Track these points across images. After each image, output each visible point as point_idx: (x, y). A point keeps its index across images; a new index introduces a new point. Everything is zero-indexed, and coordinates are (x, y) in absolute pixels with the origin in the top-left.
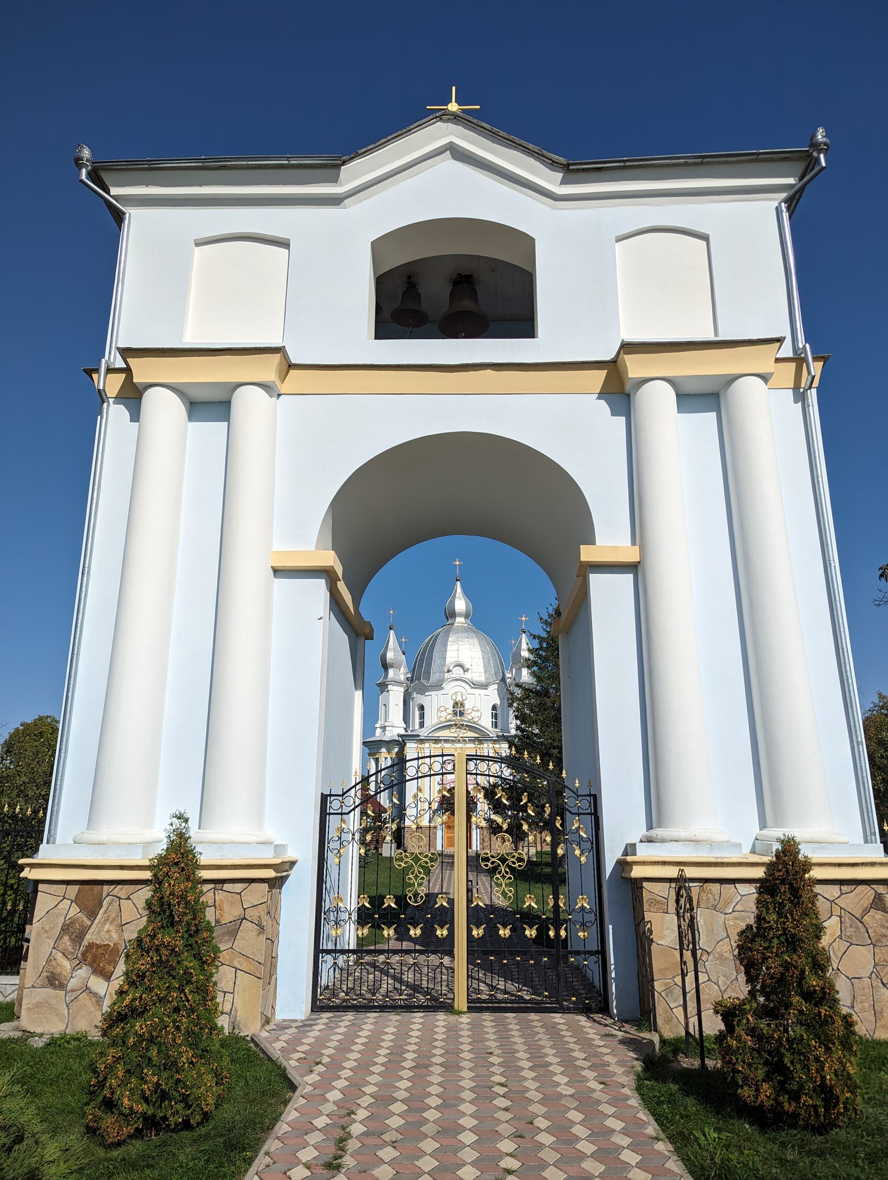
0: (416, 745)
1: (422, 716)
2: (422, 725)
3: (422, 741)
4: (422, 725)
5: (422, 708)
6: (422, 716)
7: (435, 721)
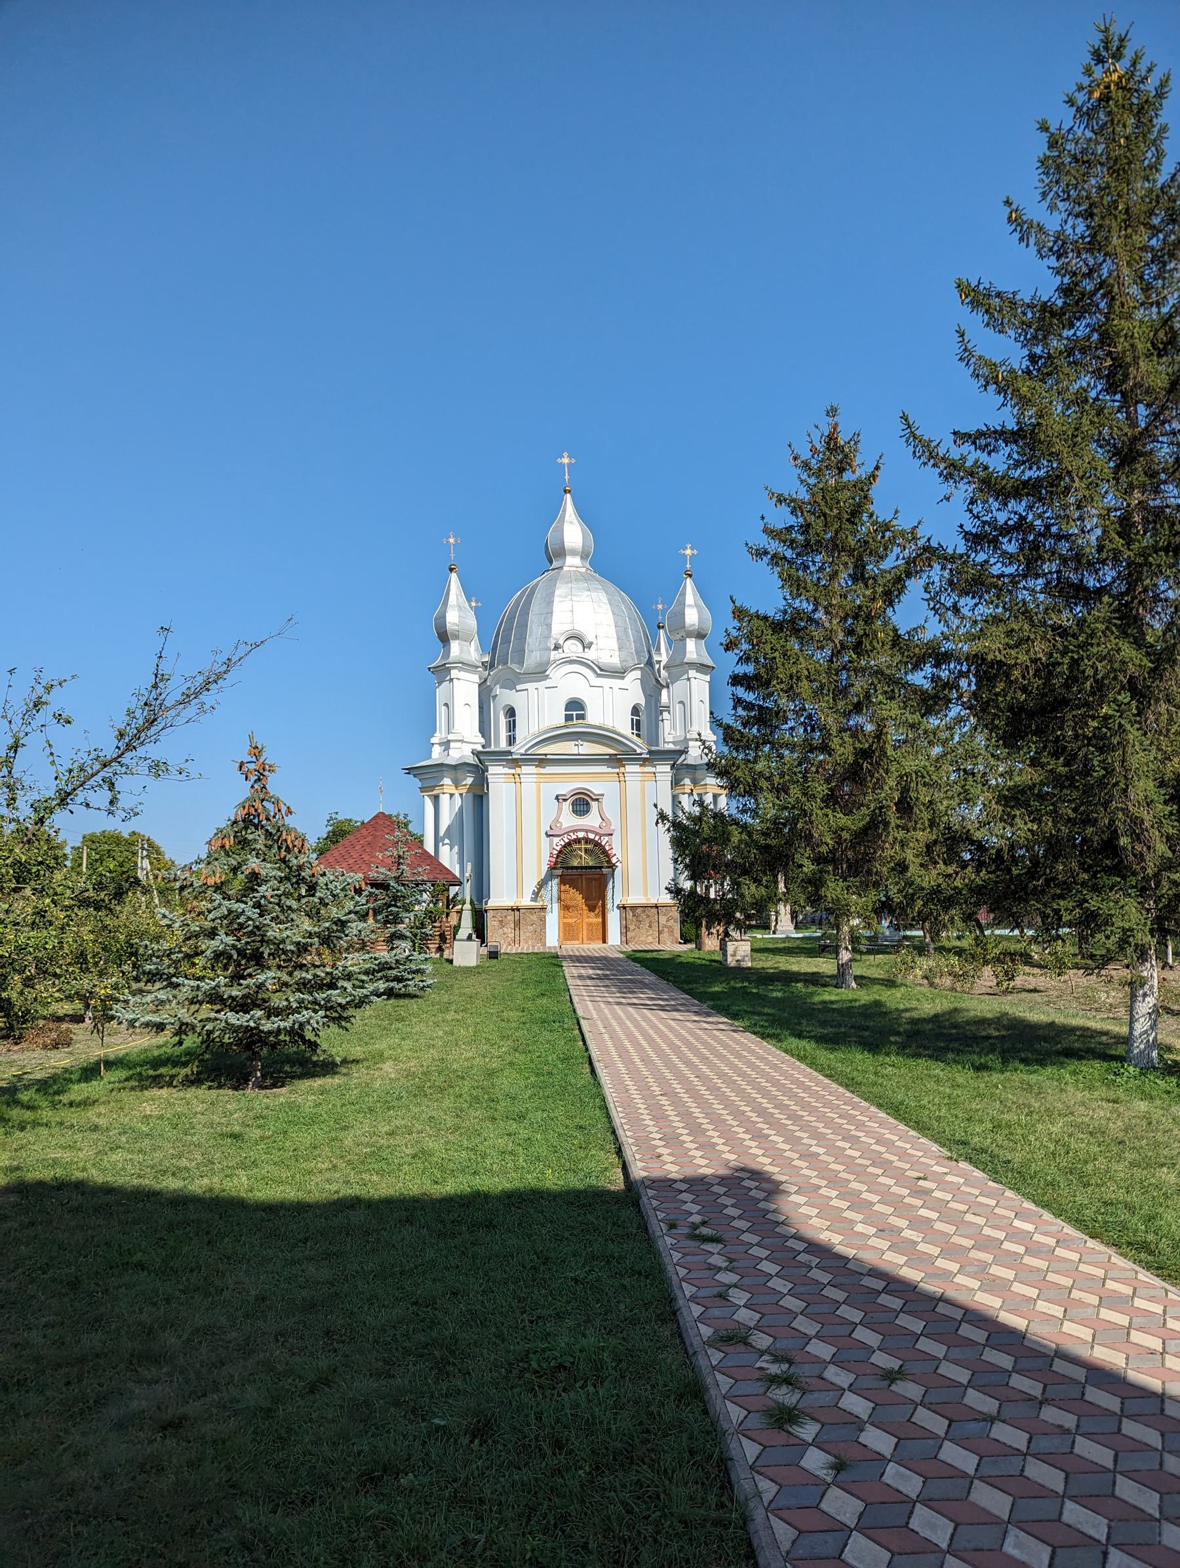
0: (506, 770)
1: (512, 726)
2: (511, 740)
3: (516, 763)
4: (511, 740)
5: (511, 712)
6: (512, 726)
7: (534, 729)
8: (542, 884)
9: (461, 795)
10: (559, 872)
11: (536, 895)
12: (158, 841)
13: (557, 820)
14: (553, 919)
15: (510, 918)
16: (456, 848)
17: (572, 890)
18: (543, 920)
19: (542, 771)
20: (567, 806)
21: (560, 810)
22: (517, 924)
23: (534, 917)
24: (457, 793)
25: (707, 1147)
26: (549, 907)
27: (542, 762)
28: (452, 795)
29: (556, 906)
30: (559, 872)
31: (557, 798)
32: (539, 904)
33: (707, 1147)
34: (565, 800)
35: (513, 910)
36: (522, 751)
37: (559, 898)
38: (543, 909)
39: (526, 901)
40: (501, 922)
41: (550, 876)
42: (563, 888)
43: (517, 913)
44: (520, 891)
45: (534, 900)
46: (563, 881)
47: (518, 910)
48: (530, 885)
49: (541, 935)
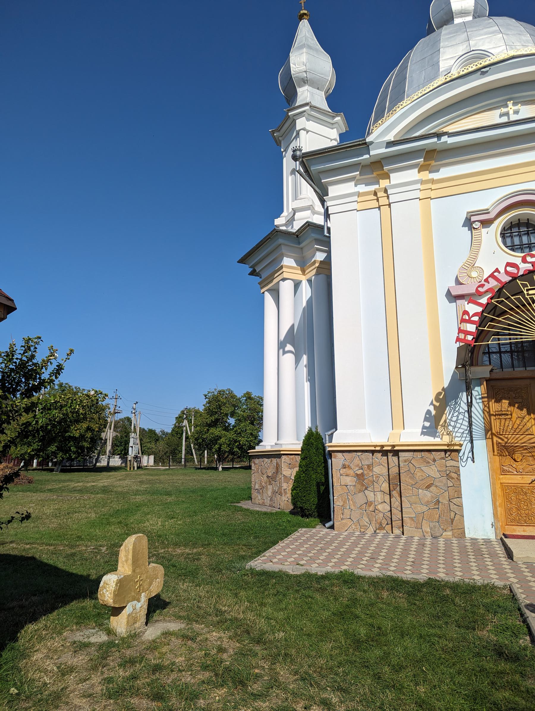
0: (362, 188)
8: (445, 399)
9: (309, 281)
10: (483, 371)
11: (434, 422)
12: (177, 413)
13: (471, 265)
14: (477, 479)
15: (380, 470)
16: (305, 359)
17: (516, 412)
18: (453, 476)
19: (435, 176)
20: (491, 236)
21: (475, 245)
22: (395, 483)
23: (433, 471)
24: (304, 279)
25: (483, 568)
26: (466, 447)
27: (433, 157)
28: (297, 285)
29: (481, 446)
30: (483, 371)
31: (468, 223)
32: (441, 440)
33: (483, 568)
34: (486, 223)
35: (385, 453)
36: (391, 137)
37: (488, 429)
38: (451, 451)
39: (412, 435)
40: (360, 477)
41: (463, 381)
42: (494, 407)
43: (393, 460)
44: (398, 419)
45: (426, 431)
46: (495, 391)
47: (396, 453)
48: (420, 400)
49: (450, 513)
